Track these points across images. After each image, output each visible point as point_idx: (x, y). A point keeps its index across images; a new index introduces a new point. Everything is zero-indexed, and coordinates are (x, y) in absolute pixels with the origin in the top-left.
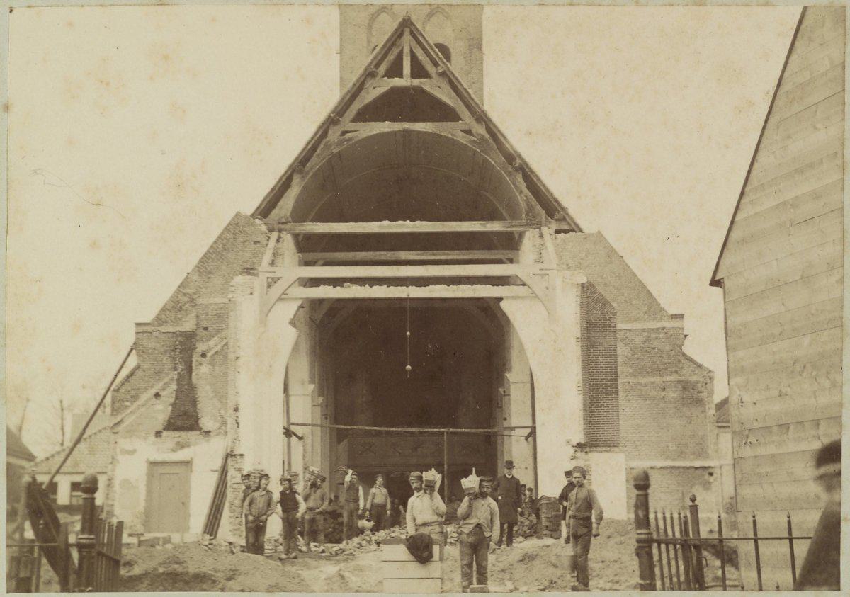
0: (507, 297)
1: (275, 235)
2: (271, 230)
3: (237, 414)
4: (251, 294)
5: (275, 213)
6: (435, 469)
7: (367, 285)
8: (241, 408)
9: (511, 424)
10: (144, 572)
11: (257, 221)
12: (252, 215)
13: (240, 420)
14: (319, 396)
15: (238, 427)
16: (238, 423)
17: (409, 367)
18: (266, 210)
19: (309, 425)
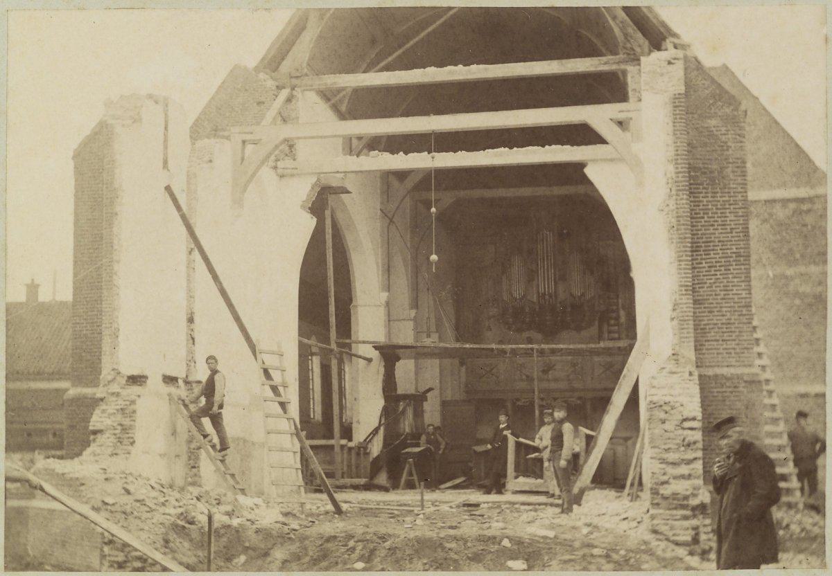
0: (594, 161)
1: (284, 93)
2: (279, 88)
3: (192, 326)
4: (211, 161)
5: (286, 66)
6: (306, 434)
7: (401, 153)
8: (197, 319)
9: (358, 338)
10: (729, 375)
11: (262, 76)
12: (257, 69)
13: (196, 336)
14: (412, 308)
15: (194, 344)
16: (193, 339)
17: (434, 257)
18: (273, 62)
19: (360, 342)
